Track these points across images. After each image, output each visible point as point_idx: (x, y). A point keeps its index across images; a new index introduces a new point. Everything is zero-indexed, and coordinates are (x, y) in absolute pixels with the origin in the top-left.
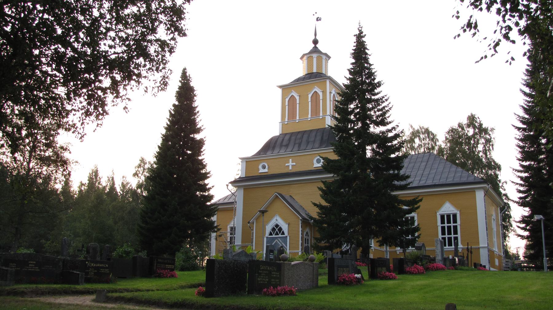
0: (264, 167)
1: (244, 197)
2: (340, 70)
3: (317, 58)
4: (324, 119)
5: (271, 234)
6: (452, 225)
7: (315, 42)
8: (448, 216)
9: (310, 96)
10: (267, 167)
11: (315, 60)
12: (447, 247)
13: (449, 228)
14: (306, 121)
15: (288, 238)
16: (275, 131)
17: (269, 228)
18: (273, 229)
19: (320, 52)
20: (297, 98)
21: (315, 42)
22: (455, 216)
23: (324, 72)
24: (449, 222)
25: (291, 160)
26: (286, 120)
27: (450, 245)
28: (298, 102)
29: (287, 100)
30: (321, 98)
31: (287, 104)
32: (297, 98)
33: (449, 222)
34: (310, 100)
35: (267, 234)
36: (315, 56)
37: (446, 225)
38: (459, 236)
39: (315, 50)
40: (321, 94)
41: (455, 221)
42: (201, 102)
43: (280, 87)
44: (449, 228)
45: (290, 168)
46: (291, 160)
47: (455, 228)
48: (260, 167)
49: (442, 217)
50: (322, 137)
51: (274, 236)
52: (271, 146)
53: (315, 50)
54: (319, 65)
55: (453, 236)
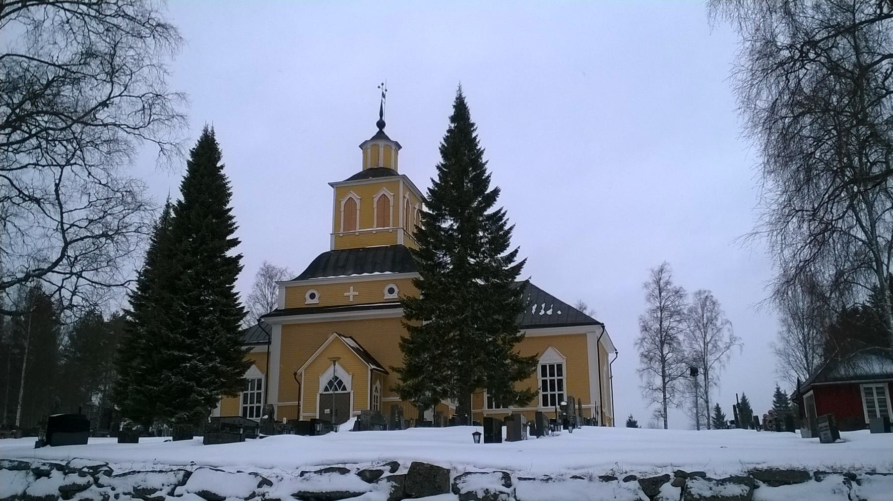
0: (312, 296)
1: (282, 340)
2: (422, 167)
3: (385, 146)
4: (395, 231)
5: (326, 389)
6: (556, 378)
7: (381, 124)
8: (552, 367)
9: (376, 200)
10: (317, 297)
11: (382, 149)
12: (550, 406)
13: (553, 389)
14: (370, 234)
15: (352, 395)
16: (325, 246)
17: (324, 381)
18: (331, 383)
19: (387, 138)
20: (358, 202)
21: (381, 124)
22: (560, 367)
23: (393, 168)
24: (552, 375)
25: (352, 288)
26: (342, 231)
27: (553, 404)
28: (358, 208)
29: (343, 203)
30: (391, 203)
31: (342, 209)
32: (358, 202)
33: (552, 375)
34: (375, 206)
35: (321, 391)
36: (381, 143)
37: (548, 378)
38: (564, 378)
39: (381, 135)
40: (391, 199)
41: (560, 374)
42: (485, 137)
43: (332, 185)
44: (553, 389)
45: (351, 300)
46: (352, 288)
47: (560, 382)
48: (307, 296)
49: (544, 368)
50: (395, 258)
51: (331, 392)
52: (321, 266)
53: (381, 135)
54: (387, 157)
55: (557, 392)
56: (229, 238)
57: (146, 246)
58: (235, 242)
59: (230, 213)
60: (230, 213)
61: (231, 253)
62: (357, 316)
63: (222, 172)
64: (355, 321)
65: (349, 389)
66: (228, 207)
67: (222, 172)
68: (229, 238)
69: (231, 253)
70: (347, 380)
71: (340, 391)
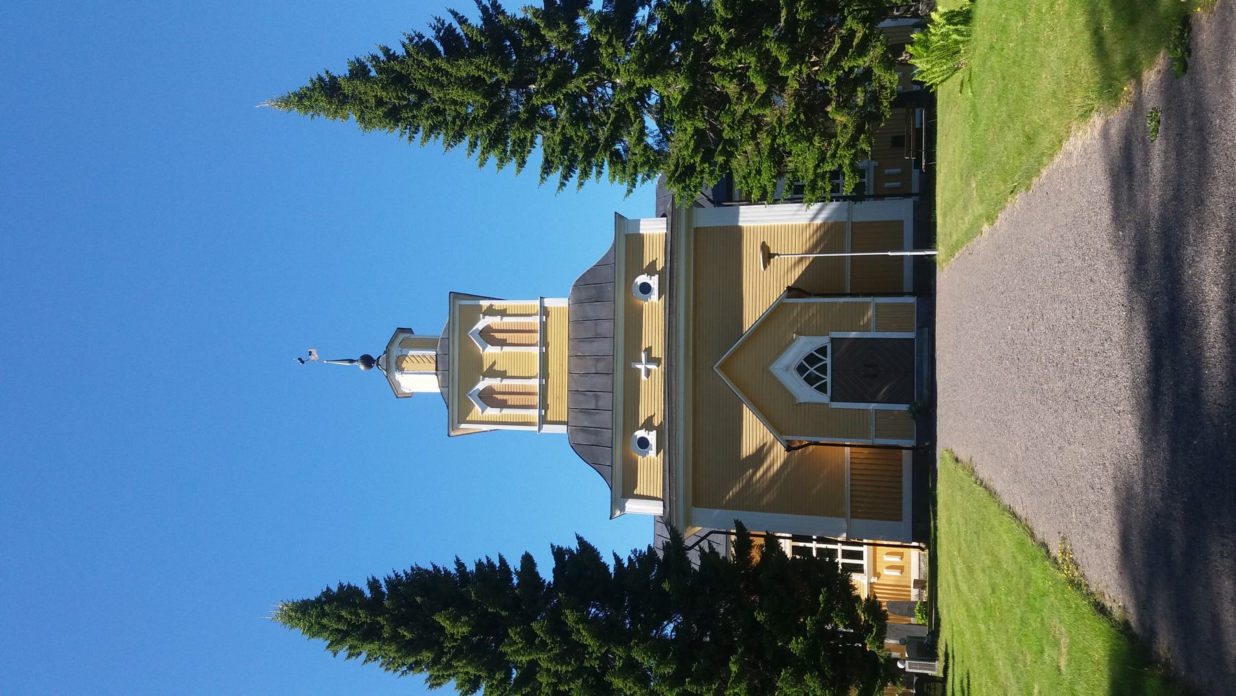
5: (822, 388)
17: (806, 393)
18: (810, 380)
35: (824, 398)
56: (368, 594)
57: (938, 229)
58: (528, 560)
59: (409, 571)
60: (409, 571)
61: (546, 570)
62: (685, 475)
63: (471, 567)
64: (694, 443)
65: (823, 341)
66: (452, 568)
67: (471, 567)
68: (368, 594)
69: (546, 570)
70: (803, 346)
71: (828, 361)
